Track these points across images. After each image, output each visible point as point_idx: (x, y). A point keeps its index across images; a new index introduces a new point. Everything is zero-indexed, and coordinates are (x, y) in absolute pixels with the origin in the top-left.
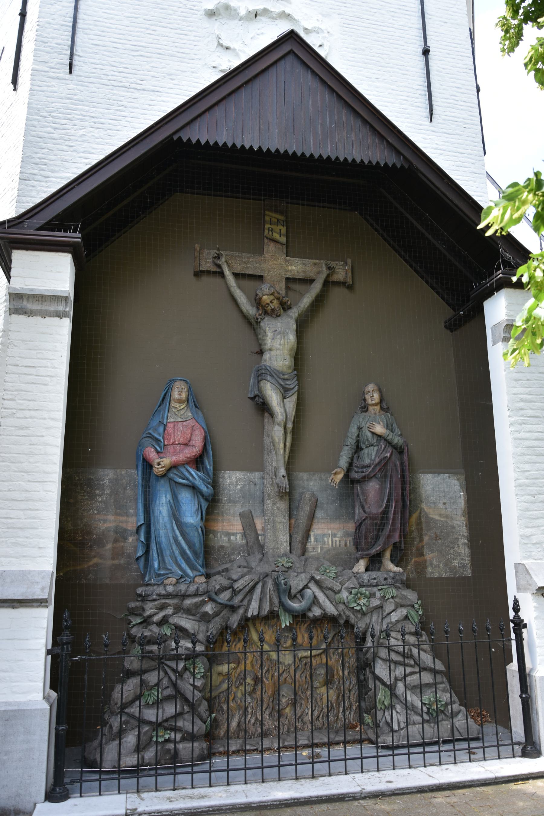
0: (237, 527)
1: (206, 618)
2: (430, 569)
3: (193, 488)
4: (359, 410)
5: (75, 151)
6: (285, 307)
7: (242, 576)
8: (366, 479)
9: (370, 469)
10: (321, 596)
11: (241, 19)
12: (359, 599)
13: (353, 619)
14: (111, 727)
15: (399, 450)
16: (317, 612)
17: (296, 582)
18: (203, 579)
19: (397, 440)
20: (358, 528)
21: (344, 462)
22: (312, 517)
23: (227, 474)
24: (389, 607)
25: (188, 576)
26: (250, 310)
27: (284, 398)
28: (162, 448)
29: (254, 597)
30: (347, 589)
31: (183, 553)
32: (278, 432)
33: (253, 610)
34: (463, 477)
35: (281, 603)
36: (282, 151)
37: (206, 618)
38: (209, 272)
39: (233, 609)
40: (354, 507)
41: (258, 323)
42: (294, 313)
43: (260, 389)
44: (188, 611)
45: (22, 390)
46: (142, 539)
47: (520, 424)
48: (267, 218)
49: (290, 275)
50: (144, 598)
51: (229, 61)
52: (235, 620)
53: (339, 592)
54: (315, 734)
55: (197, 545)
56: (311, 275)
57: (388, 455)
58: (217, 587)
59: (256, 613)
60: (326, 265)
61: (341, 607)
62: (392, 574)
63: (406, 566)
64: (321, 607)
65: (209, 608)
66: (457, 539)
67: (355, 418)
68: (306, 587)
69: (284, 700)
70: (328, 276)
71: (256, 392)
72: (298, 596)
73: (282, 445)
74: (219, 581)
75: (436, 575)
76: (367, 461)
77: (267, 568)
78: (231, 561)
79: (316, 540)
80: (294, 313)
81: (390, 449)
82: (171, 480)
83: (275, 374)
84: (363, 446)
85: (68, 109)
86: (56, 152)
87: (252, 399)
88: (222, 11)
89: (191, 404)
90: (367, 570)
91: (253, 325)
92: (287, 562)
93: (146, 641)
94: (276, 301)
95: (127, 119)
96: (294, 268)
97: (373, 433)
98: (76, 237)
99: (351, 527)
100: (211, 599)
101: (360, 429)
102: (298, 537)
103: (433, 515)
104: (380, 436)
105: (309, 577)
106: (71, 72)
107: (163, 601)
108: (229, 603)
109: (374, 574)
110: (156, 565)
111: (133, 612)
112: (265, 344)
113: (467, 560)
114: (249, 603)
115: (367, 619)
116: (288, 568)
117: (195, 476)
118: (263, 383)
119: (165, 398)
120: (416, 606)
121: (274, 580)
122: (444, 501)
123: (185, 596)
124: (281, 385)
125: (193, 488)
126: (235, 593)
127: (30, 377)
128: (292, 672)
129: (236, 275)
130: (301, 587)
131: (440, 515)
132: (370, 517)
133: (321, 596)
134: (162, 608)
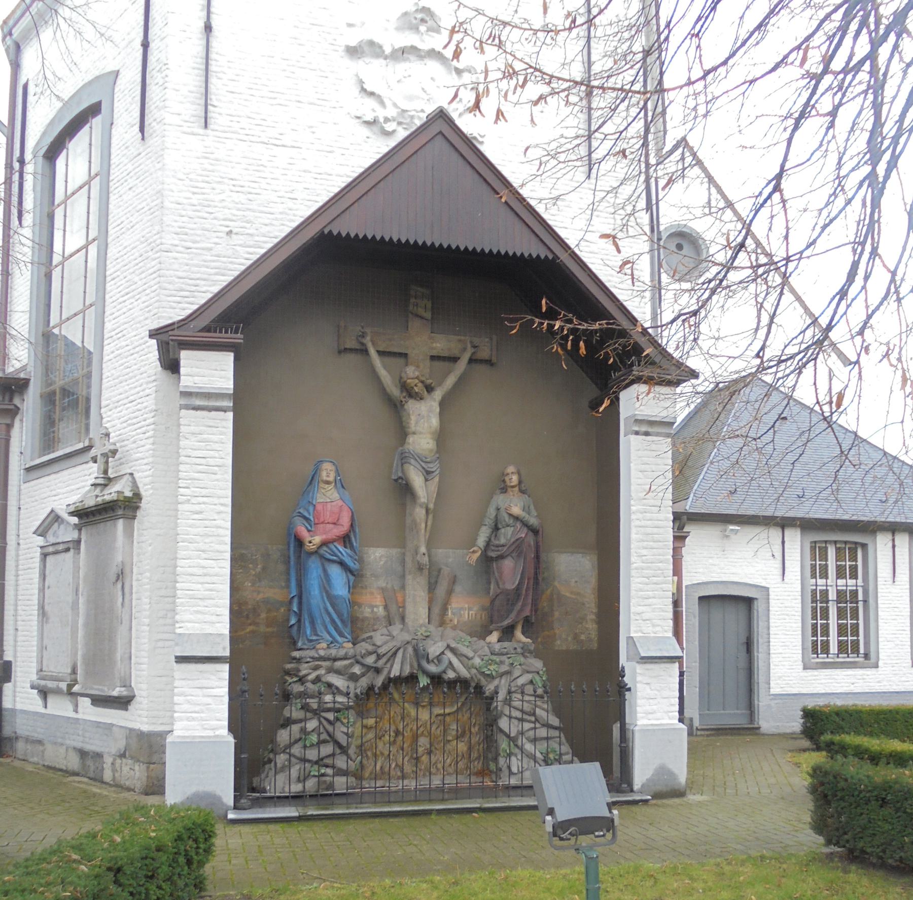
0: (378, 601)
1: (354, 678)
2: (558, 642)
3: (342, 564)
4: (498, 491)
5: (215, 218)
6: (430, 389)
7: (385, 643)
8: (502, 557)
9: (505, 549)
10: (455, 662)
11: (386, 58)
12: (490, 665)
13: (483, 682)
14: (276, 764)
15: (535, 531)
16: (451, 675)
17: (434, 649)
18: (350, 645)
19: (533, 521)
20: (492, 602)
21: (481, 541)
22: (450, 592)
23: (371, 550)
24: (517, 673)
25: (337, 642)
26: (395, 392)
27: (426, 480)
28: (312, 524)
29: (396, 660)
30: (479, 656)
31: (333, 622)
32: (420, 513)
33: (395, 672)
34: (595, 558)
35: (419, 665)
36: (429, 244)
37: (354, 678)
38: (351, 350)
39: (378, 671)
40: (490, 583)
41: (403, 406)
42: (438, 394)
43: (403, 471)
44: (338, 672)
45: (195, 479)
46: (295, 609)
47: (641, 513)
48: (412, 293)
49: (434, 353)
50: (298, 660)
51: (374, 110)
52: (379, 681)
53: (472, 658)
54: (446, 777)
55: (345, 615)
56: (455, 352)
57: (523, 535)
58: (363, 652)
59: (398, 674)
60: (471, 342)
61: (474, 671)
62: (521, 645)
63: (537, 638)
64: (454, 670)
65: (357, 670)
66: (586, 615)
67: (495, 497)
68: (443, 653)
69: (420, 750)
70: (473, 353)
71: (400, 474)
72: (435, 661)
73: (423, 525)
74: (364, 647)
75: (564, 648)
76: (503, 541)
77: (407, 637)
78: (374, 631)
79: (453, 614)
80: (438, 394)
81: (525, 530)
82: (322, 557)
83: (420, 458)
84: (500, 526)
85: (205, 170)
86: (196, 220)
87: (396, 480)
88: (366, 49)
89: (339, 485)
90: (499, 641)
91: (396, 408)
92: (426, 631)
93: (303, 695)
94: (420, 385)
95: (267, 181)
96: (438, 345)
97: (510, 515)
98: (238, 338)
99: (486, 601)
100: (358, 662)
101: (498, 509)
102: (436, 610)
103: (565, 592)
104: (517, 518)
105: (445, 645)
106: (206, 126)
107: (317, 663)
108: (374, 665)
109: (506, 644)
110: (308, 632)
111: (288, 673)
112: (409, 427)
113: (594, 635)
114: (392, 666)
115: (496, 682)
116: (427, 637)
117: (343, 552)
118: (406, 466)
119: (313, 479)
120: (541, 672)
121: (414, 647)
122: (576, 579)
123: (335, 660)
124: (423, 468)
125: (342, 564)
126: (379, 657)
127: (201, 467)
128: (428, 726)
129: (381, 353)
130: (438, 654)
131: (572, 593)
132: (506, 593)
133: (455, 662)
134: (316, 668)
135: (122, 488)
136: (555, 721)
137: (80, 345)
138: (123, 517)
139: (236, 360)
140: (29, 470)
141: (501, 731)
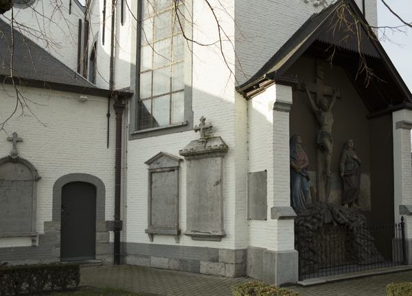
16: (343, 222)
44: (308, 222)
101: (347, 156)
129: (310, 92)
135: (215, 144)
136: (373, 239)
137: (379, 57)
138: (220, 156)
139: (294, 91)
140: (133, 135)
141: (357, 243)
